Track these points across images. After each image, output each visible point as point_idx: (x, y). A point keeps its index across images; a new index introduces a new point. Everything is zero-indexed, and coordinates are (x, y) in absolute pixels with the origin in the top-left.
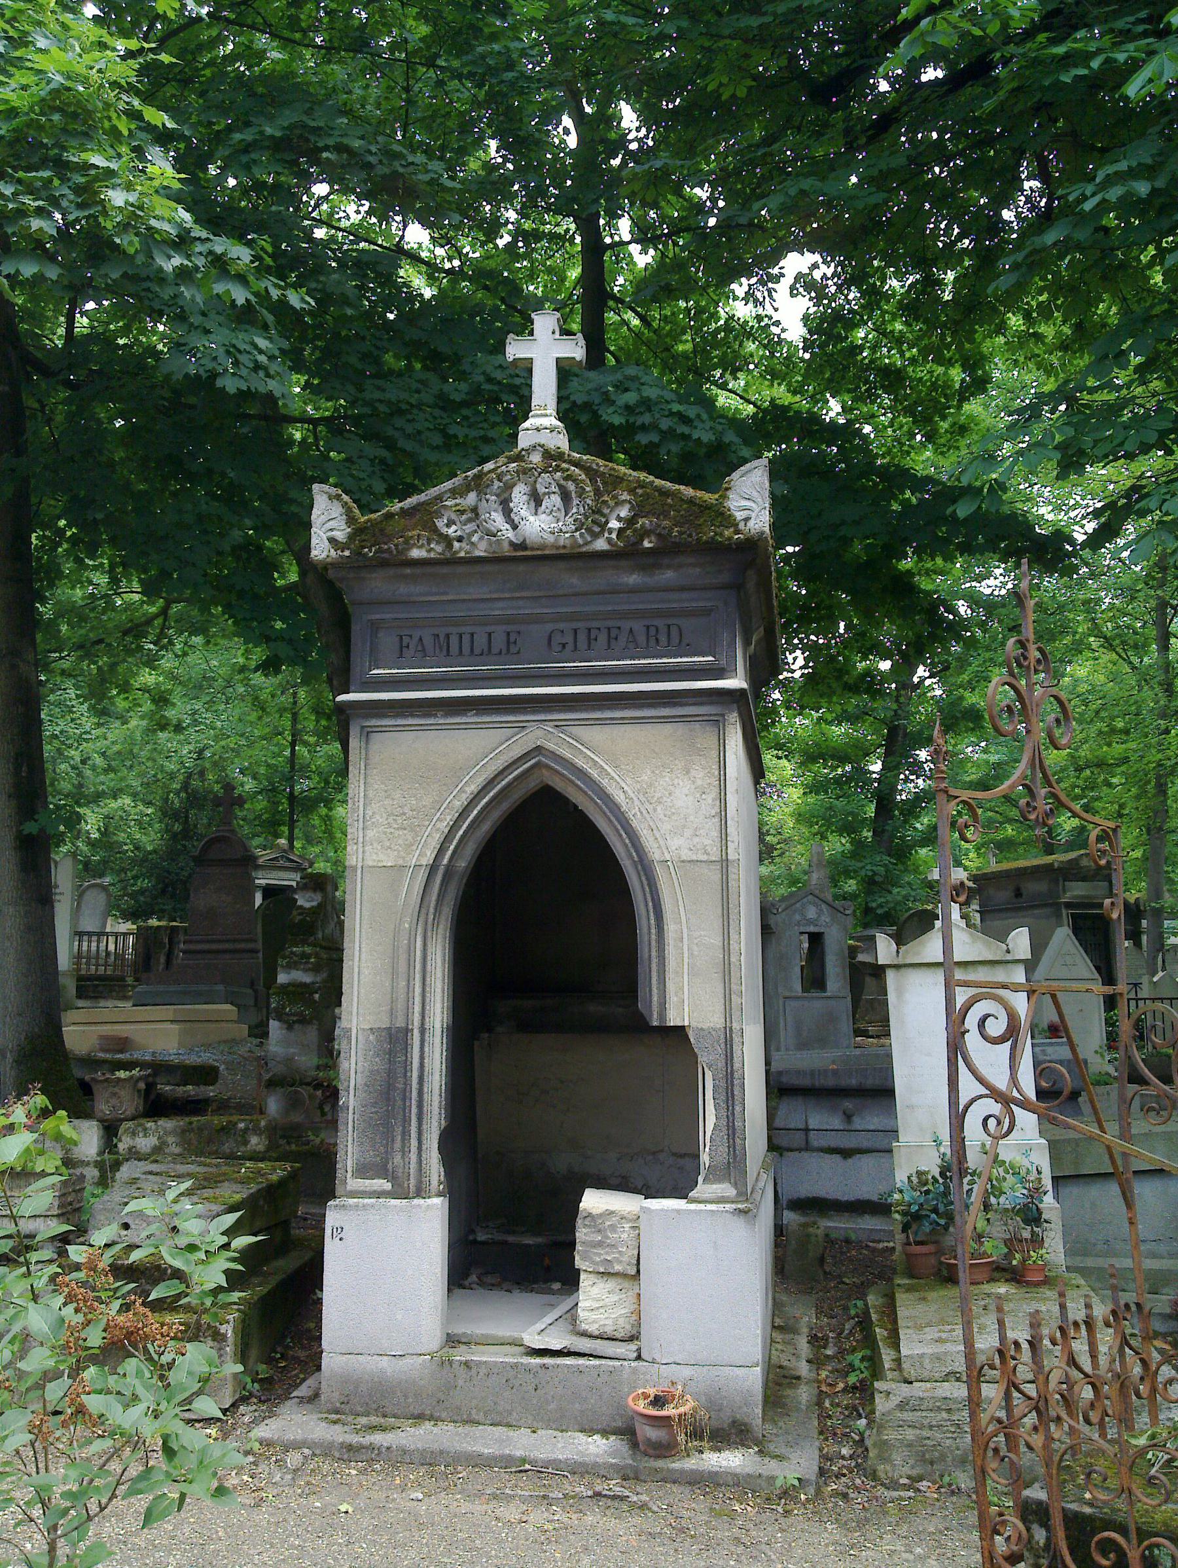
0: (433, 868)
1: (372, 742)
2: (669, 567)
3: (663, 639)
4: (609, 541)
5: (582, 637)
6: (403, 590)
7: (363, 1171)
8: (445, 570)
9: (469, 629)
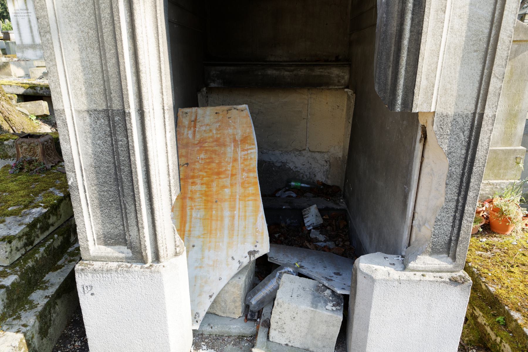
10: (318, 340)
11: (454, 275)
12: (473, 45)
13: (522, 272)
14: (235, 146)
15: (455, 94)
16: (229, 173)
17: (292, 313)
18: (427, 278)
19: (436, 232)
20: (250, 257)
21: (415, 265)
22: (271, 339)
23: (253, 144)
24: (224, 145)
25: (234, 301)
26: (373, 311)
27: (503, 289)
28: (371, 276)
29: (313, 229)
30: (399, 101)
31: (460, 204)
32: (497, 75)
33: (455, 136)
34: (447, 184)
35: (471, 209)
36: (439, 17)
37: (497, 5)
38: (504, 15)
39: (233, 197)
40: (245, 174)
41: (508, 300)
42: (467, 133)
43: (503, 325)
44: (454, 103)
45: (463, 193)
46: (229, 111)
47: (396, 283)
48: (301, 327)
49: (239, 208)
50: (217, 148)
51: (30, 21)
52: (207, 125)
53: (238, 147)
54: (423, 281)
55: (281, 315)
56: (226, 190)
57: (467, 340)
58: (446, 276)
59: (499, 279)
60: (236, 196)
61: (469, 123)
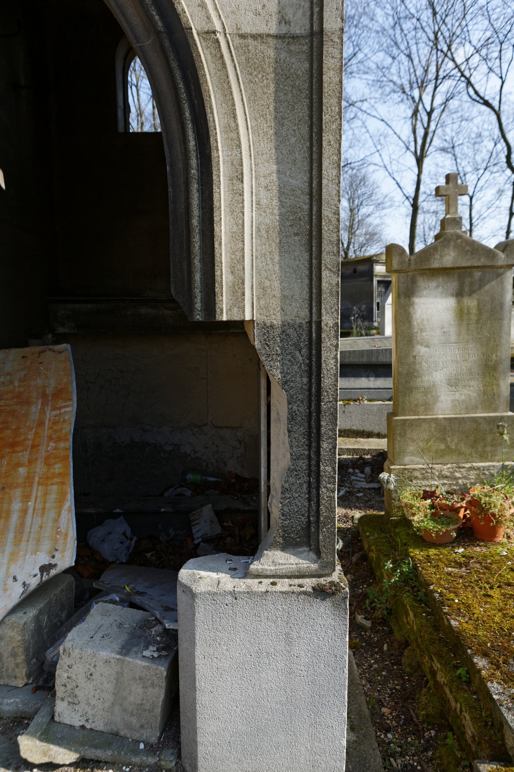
10: (132, 714)
11: (322, 581)
12: (291, 226)
13: (504, 595)
14: (43, 404)
15: (278, 295)
16: (30, 443)
17: (88, 666)
18: (279, 588)
19: (286, 509)
20: (42, 576)
21: (260, 567)
22: (57, 719)
23: (71, 400)
24: (28, 403)
25: (14, 655)
26: (198, 652)
27: (470, 622)
28: (189, 587)
29: (203, 541)
30: (198, 305)
31: (313, 463)
32: (329, 266)
33: (289, 357)
34: (289, 431)
35: (329, 469)
36: (235, 188)
37: (314, 173)
38: (323, 185)
39: (29, 480)
40: (52, 444)
41: (474, 640)
43: (465, 682)
44: (279, 308)
45: (314, 444)
46: (42, 354)
47: (229, 597)
48: (102, 691)
49: (36, 497)
50: (16, 407)
52: (8, 374)
53: (48, 405)
54: (272, 593)
55: (70, 670)
56: (20, 469)
57: (424, 715)
58: (309, 583)
59: (469, 607)
60: (34, 477)
61: (305, 337)
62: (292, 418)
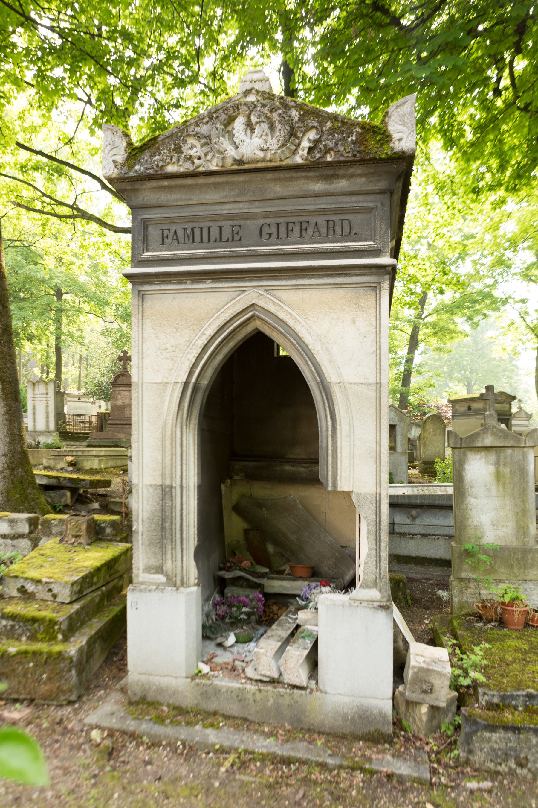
0: (186, 384)
1: (145, 301)
2: (343, 177)
3: (338, 229)
4: (302, 156)
5: (283, 229)
6: (164, 197)
7: (148, 569)
8: (189, 181)
9: (207, 224)
42: (374, 505)
51: (47, 406)
62: (369, 532)
